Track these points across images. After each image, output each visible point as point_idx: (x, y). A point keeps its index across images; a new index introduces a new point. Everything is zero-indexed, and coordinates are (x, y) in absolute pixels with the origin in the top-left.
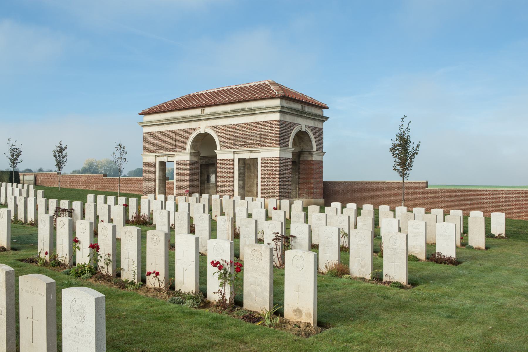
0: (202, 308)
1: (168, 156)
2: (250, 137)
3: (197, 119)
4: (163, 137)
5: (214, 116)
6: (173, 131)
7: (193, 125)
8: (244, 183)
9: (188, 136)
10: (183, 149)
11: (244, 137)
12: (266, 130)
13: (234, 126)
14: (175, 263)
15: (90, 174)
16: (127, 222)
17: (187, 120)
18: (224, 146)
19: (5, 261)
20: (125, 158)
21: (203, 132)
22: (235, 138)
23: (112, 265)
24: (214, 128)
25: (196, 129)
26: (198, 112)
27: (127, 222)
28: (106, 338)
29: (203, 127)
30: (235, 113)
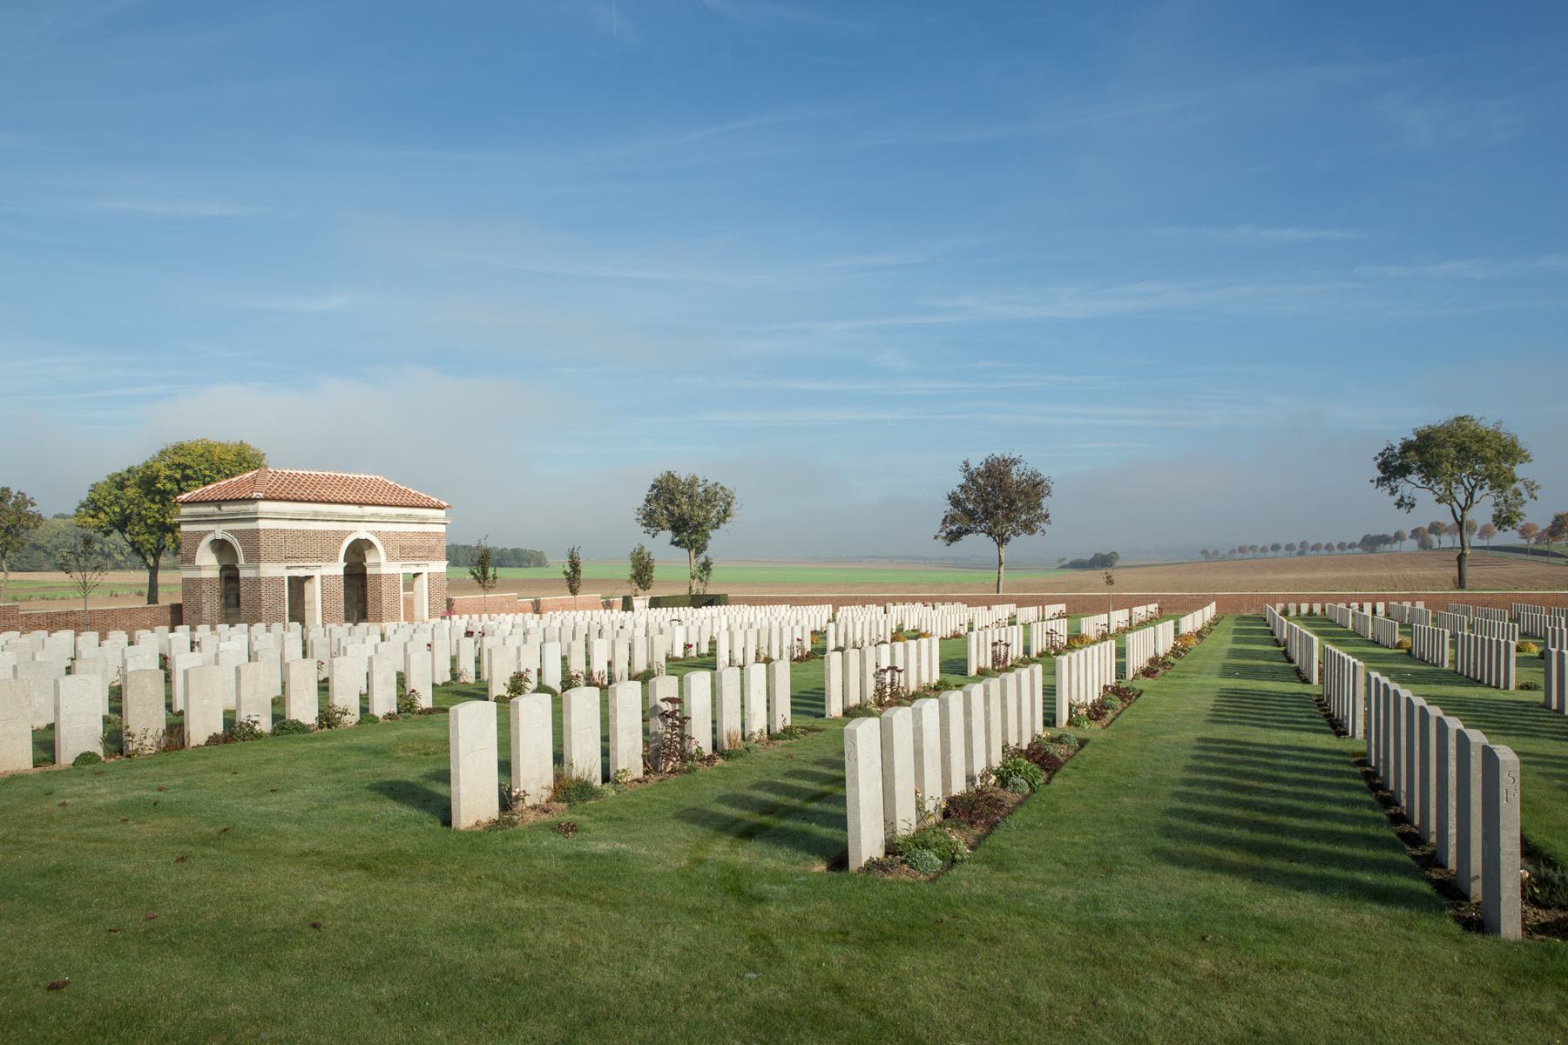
0: (1283, 778)
1: (307, 567)
2: (420, 548)
3: (358, 520)
4: (301, 539)
6: (316, 532)
8: (1222, 559)
9: (341, 541)
10: (332, 558)
11: (413, 549)
12: (433, 542)
13: (399, 534)
14: (1044, 714)
15: (7, 604)
16: (757, 660)
17: (342, 520)
18: (390, 558)
19: (1205, 963)
20: (654, 536)
21: (363, 537)
22: (402, 548)
23: (1518, 781)
24: (376, 534)
25: (351, 532)
27: (757, 660)
28: (594, 855)
29: (362, 532)
30: (408, 520)
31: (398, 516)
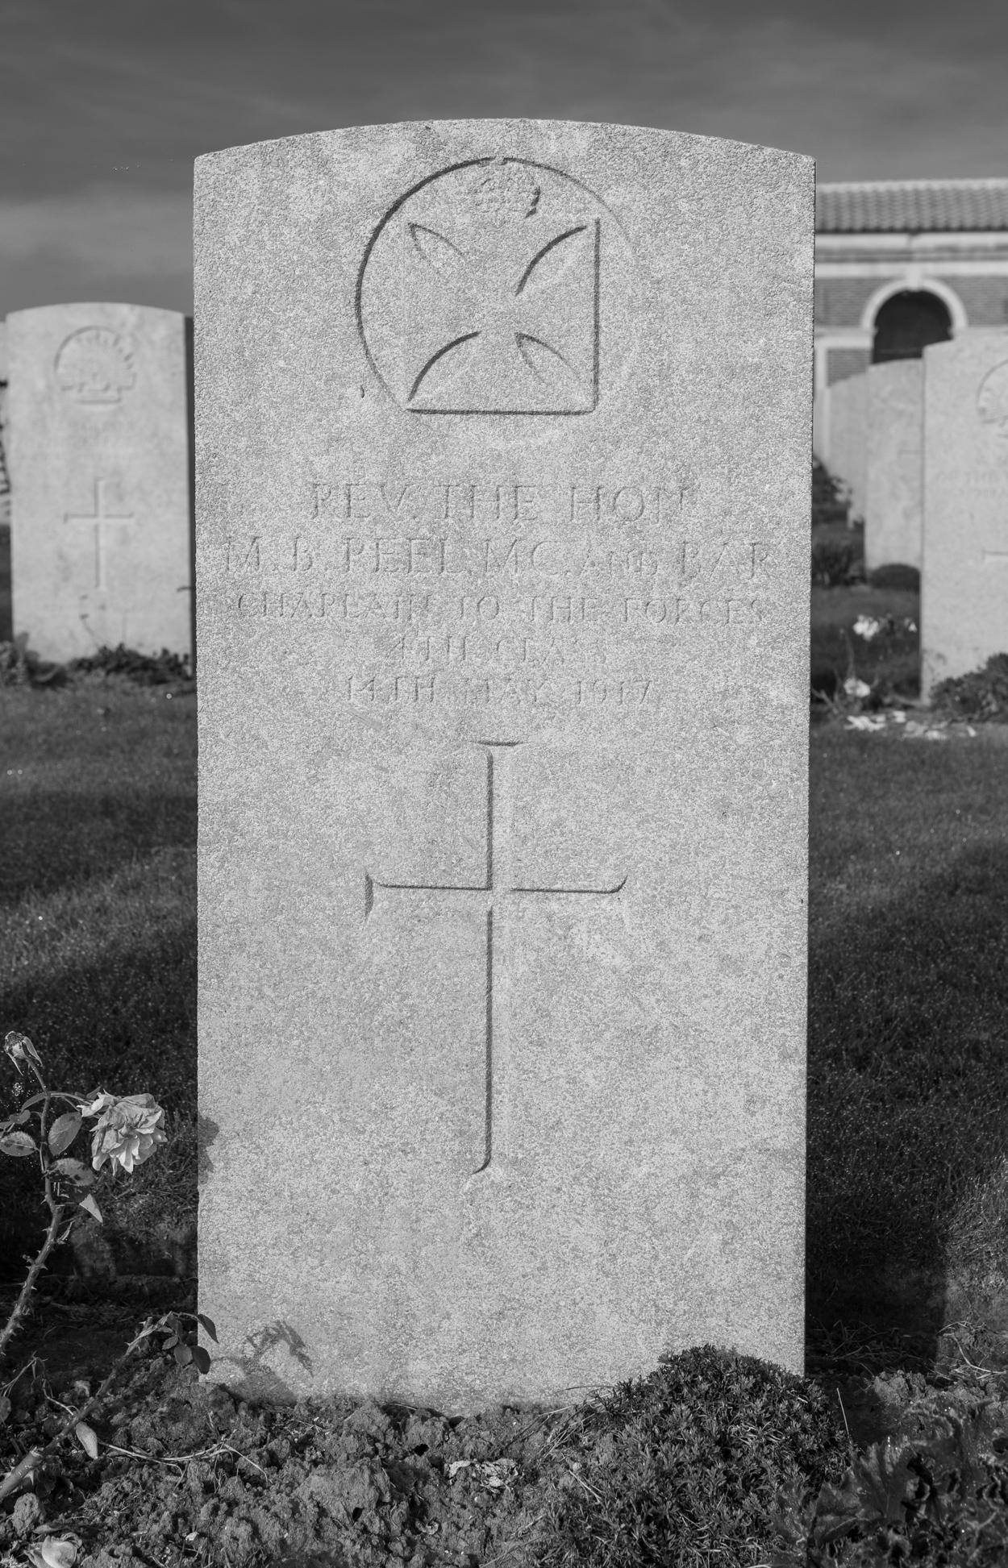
3: (905, 256)
5: (954, 253)
7: (883, 269)
10: (851, 320)
26: (898, 241)
29: (914, 277)
31: (940, 249)
